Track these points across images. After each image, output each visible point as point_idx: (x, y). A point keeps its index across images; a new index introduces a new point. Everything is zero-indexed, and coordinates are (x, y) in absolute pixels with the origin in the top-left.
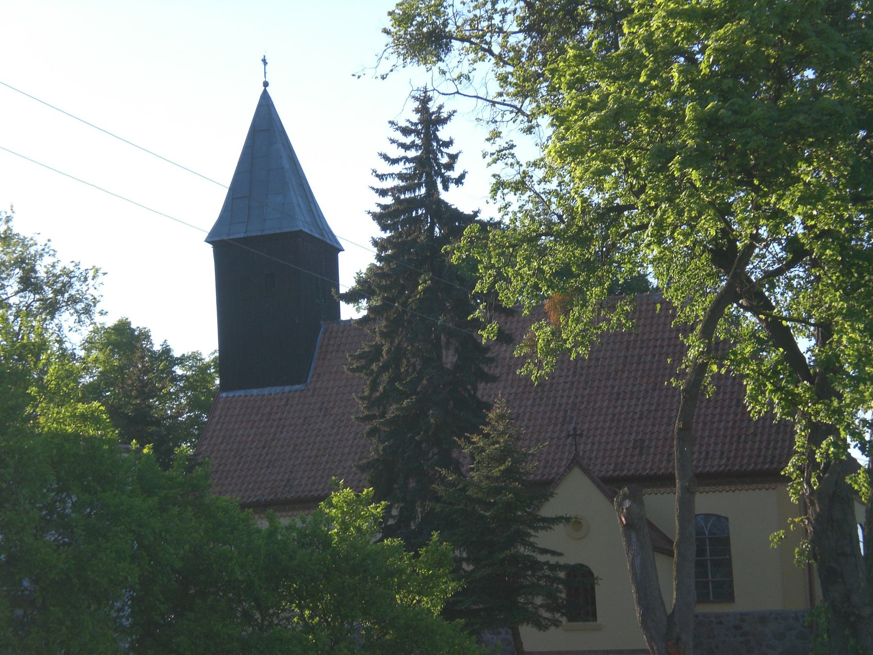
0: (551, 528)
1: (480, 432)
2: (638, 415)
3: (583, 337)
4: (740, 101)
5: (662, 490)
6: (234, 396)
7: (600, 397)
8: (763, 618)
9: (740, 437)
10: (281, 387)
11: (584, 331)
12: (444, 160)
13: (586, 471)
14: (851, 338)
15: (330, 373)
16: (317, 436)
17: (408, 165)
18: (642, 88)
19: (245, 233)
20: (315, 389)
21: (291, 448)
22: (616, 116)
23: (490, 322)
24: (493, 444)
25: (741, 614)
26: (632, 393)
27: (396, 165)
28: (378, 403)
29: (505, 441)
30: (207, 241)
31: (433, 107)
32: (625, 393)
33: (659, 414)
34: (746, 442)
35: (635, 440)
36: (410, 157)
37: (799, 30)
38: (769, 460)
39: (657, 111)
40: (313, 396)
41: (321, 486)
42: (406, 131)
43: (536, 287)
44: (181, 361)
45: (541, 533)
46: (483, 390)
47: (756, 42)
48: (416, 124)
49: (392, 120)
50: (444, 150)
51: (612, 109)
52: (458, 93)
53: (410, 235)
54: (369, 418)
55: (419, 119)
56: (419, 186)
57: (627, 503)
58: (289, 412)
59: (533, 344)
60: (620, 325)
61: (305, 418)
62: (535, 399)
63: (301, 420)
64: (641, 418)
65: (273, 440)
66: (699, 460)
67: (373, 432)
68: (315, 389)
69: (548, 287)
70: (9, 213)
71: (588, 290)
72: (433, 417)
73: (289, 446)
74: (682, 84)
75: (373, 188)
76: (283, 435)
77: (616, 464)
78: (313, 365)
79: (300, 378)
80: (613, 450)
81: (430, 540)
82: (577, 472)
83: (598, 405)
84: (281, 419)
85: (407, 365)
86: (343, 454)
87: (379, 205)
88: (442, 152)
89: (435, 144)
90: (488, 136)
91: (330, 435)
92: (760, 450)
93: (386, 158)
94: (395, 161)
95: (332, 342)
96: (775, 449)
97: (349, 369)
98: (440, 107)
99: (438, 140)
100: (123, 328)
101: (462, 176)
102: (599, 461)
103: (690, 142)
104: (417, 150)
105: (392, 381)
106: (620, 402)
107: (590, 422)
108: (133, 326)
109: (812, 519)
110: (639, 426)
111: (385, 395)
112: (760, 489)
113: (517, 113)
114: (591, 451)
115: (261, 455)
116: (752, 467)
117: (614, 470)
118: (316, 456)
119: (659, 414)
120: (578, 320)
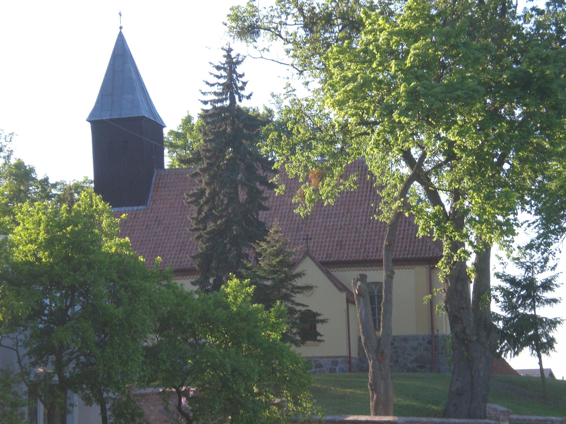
0: (303, 292)
1: (265, 240)
3: (332, 194)
4: (427, 82)
5: (352, 269)
7: (317, 217)
8: (405, 339)
10: (132, 207)
12: (240, 85)
13: (313, 259)
14: (476, 201)
17: (219, 87)
18: (374, 70)
19: (110, 116)
20: (152, 209)
21: (139, 243)
22: (362, 86)
24: (273, 247)
26: (336, 214)
28: (204, 221)
29: (280, 246)
30: (87, 120)
31: (233, 54)
32: (332, 214)
33: (351, 226)
35: (338, 241)
36: (221, 83)
37: (455, 44)
39: (380, 82)
40: (151, 213)
42: (218, 68)
43: (306, 166)
44: (54, 186)
45: (298, 295)
46: (262, 216)
47: (434, 51)
48: (224, 64)
50: (240, 79)
51: (360, 83)
52: (262, 57)
53: (221, 127)
54: (196, 230)
56: (226, 99)
57: (359, 283)
58: (137, 222)
59: (303, 196)
60: (351, 187)
61: (147, 226)
63: (145, 226)
64: (340, 229)
66: (373, 252)
67: (198, 238)
68: (152, 209)
71: (334, 168)
74: (396, 71)
76: (134, 235)
77: (327, 255)
78: (151, 194)
79: (143, 202)
80: (325, 246)
81: (275, 305)
85: (218, 200)
86: (170, 247)
87: (203, 110)
88: (238, 81)
89: (235, 76)
90: (285, 87)
91: (162, 236)
92: (406, 247)
93: (207, 83)
95: (161, 181)
96: (414, 246)
97: (186, 202)
99: (235, 73)
100: (20, 165)
101: (251, 95)
103: (403, 104)
104: (225, 79)
105: (210, 210)
106: (329, 219)
108: (26, 164)
110: (339, 233)
112: (409, 269)
113: (300, 74)
116: (401, 256)
117: (326, 258)
118: (155, 248)
120: (328, 185)
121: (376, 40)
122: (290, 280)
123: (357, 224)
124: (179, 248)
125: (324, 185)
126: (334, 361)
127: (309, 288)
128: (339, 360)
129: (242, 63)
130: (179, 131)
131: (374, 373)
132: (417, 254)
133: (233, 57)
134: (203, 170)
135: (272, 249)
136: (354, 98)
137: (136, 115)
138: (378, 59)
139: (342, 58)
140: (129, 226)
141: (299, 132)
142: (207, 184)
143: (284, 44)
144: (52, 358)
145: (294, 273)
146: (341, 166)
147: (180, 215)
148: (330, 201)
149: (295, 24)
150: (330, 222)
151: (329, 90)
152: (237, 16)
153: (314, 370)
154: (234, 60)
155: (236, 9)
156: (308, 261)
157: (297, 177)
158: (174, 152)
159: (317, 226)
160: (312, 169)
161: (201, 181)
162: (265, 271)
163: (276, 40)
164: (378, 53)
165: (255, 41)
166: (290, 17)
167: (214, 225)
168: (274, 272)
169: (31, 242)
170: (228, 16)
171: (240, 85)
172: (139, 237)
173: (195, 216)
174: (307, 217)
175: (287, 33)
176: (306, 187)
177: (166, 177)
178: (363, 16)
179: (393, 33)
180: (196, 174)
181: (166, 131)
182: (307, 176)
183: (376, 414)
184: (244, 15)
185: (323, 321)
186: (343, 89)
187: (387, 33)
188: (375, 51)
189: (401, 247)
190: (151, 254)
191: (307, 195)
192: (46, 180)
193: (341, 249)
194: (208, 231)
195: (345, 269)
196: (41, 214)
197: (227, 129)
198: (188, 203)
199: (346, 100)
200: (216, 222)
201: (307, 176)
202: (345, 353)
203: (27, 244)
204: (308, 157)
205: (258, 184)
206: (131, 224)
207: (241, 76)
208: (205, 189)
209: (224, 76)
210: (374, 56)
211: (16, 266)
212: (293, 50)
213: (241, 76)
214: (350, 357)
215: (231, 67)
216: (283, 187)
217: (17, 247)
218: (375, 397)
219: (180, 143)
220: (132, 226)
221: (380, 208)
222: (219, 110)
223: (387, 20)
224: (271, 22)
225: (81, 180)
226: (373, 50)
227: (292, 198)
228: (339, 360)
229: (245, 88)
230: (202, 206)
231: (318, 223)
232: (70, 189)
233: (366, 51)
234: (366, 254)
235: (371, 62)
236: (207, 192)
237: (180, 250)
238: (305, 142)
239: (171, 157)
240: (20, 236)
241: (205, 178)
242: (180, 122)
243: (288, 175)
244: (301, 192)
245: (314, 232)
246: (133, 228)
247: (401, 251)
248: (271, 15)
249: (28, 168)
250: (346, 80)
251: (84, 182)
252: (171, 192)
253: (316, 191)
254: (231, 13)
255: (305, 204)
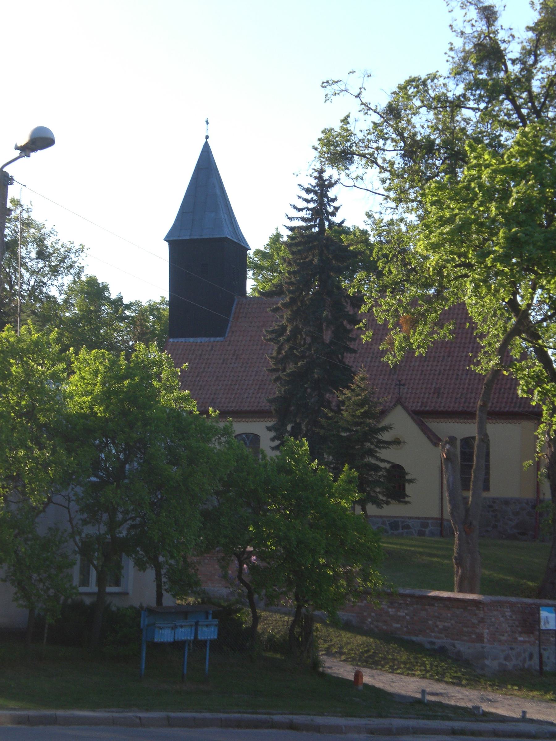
0: (389, 448)
1: (348, 388)
2: (437, 372)
3: (423, 343)
5: (450, 420)
6: (178, 342)
8: (506, 502)
9: (500, 389)
11: (424, 339)
13: (405, 408)
15: (241, 331)
16: (232, 372)
17: (308, 212)
22: (460, 229)
23: (367, 330)
25: (494, 499)
27: (301, 212)
28: (282, 361)
30: (165, 240)
31: (326, 176)
32: (430, 357)
34: (504, 393)
35: (435, 389)
38: (518, 405)
40: (229, 345)
41: (234, 404)
42: (308, 191)
43: (396, 310)
44: (128, 307)
45: (383, 451)
46: (349, 359)
48: (315, 187)
49: (300, 183)
50: (332, 204)
55: (316, 183)
56: (314, 226)
57: (448, 446)
58: (213, 355)
59: (392, 344)
61: (224, 360)
62: (372, 358)
63: (221, 361)
64: (439, 374)
65: (203, 372)
67: (278, 379)
69: (404, 311)
70: (30, 206)
72: (317, 374)
73: (213, 377)
74: (497, 215)
75: (285, 226)
79: (221, 333)
82: (399, 409)
83: (413, 364)
84: (208, 359)
86: (248, 385)
88: (330, 205)
89: (326, 200)
91: (240, 372)
93: (295, 208)
94: (300, 210)
95: (241, 311)
98: (331, 177)
99: (327, 197)
100: (92, 282)
102: (411, 400)
104: (314, 203)
105: (291, 349)
107: (407, 375)
108: (99, 281)
109: (549, 455)
110: (437, 379)
111: (286, 357)
114: (407, 393)
115: (195, 381)
117: (421, 406)
118: (231, 385)
119: (451, 372)
121: (480, 177)
122: (376, 434)
123: (459, 370)
124: (258, 387)
125: (416, 334)
126: (424, 522)
127: (397, 442)
128: (430, 522)
129: (335, 186)
130: (265, 251)
131: (460, 545)
132: (524, 408)
133: (324, 179)
134: (285, 305)
135: (356, 398)
136: (451, 242)
137: (218, 236)
138: (480, 199)
139: (441, 194)
140: (204, 359)
141: (390, 272)
142: (289, 320)
143: (380, 172)
144: (105, 517)
145: (380, 426)
146: (436, 312)
147: (260, 349)
148: (422, 350)
149: (395, 150)
150: (428, 366)
151: (423, 230)
152: (329, 141)
153: (400, 531)
154: (326, 183)
155: (329, 131)
156: (399, 410)
157: (386, 322)
158: (259, 274)
159: (413, 370)
160: (403, 313)
161: (282, 317)
162: (348, 422)
163: (371, 167)
164: (480, 191)
165: (348, 169)
166: (389, 142)
167: (295, 367)
168: (358, 424)
169: (88, 393)
170: (319, 140)
171: (330, 210)
172: (215, 372)
173: (274, 355)
174: (395, 366)
175: (384, 160)
176: (396, 333)
177: (247, 306)
178: (467, 148)
179: (498, 171)
180: (277, 309)
181: (250, 253)
182: (398, 321)
183: (461, 591)
184: (337, 139)
185: (410, 481)
186: (439, 231)
187: (490, 171)
188: (477, 189)
189: (508, 398)
190: (226, 391)
191: (396, 342)
192: (120, 299)
193: (438, 398)
194: (288, 373)
195: (442, 420)
196: (98, 364)
197: (314, 260)
198: (267, 340)
199: (442, 244)
200: (296, 364)
201: (398, 321)
202: (436, 514)
203: (83, 396)
204: (400, 300)
205: (345, 322)
206: (206, 357)
207: (333, 200)
208: (287, 326)
209: (315, 200)
210: (476, 194)
211: (69, 418)
212: (390, 179)
213: (333, 200)
214: (442, 519)
215: (322, 190)
216: (370, 333)
217: (71, 398)
218: (460, 571)
219: (266, 264)
220: (208, 359)
221: (479, 358)
222: (306, 239)
223: (494, 155)
224: (367, 147)
225: (158, 300)
226: (475, 188)
227: (380, 345)
228: (430, 522)
229: (337, 213)
230: (283, 344)
231: (414, 366)
232: (146, 310)
233: (468, 188)
234: (467, 404)
235: (473, 200)
236: (289, 329)
237: (259, 389)
238: (397, 284)
239: (256, 280)
240: (77, 386)
241: (287, 313)
242: (267, 241)
243: (377, 320)
244: (389, 339)
245: (409, 377)
246: (209, 361)
247: (506, 403)
248: (368, 139)
249: (101, 286)
250: (443, 221)
251: (160, 304)
252: (251, 323)
253: (407, 338)
254: (322, 136)
255: (394, 352)
